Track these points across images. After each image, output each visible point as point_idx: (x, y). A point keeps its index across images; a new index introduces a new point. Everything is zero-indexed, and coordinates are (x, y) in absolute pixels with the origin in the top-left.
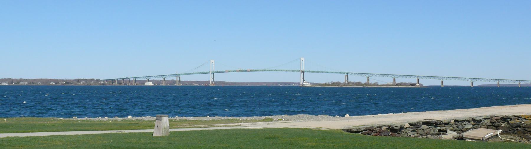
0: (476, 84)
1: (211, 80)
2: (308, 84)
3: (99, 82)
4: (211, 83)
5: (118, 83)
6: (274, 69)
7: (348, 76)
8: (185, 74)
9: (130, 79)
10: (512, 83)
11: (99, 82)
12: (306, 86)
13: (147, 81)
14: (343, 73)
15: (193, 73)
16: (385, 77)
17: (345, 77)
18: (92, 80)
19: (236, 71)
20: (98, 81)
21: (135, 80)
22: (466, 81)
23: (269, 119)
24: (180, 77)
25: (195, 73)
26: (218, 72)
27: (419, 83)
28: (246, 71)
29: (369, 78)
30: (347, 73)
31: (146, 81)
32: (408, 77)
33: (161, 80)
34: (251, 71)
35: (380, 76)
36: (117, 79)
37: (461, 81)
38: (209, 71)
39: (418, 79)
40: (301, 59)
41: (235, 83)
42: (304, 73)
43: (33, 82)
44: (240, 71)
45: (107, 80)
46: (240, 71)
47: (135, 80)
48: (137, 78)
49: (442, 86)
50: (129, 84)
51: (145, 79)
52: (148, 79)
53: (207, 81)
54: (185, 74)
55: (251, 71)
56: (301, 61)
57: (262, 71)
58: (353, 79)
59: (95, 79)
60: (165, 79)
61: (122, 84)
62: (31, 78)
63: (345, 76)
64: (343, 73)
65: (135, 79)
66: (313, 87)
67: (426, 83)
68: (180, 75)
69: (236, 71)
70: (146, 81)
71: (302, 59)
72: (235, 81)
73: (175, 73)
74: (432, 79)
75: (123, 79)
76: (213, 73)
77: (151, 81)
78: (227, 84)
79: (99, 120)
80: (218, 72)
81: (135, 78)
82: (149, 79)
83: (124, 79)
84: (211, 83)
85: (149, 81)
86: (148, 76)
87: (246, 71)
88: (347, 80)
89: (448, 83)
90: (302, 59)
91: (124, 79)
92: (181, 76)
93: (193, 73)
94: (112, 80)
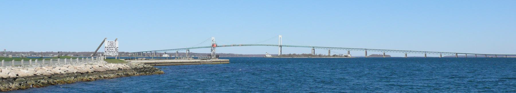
0: (443, 56)
2: (269, 55)
3: (128, 55)
5: (143, 55)
6: (198, 47)
7: (314, 49)
8: (193, 48)
9: (148, 52)
10: (451, 55)
11: (128, 55)
12: (268, 57)
13: (165, 54)
14: (311, 47)
15: (199, 48)
16: (342, 50)
17: (312, 50)
18: (123, 53)
19: (230, 46)
20: (127, 53)
21: (156, 53)
22: (401, 53)
24: (189, 50)
25: (263, 45)
26: (284, 46)
28: (238, 46)
29: (330, 51)
30: (313, 47)
31: (163, 54)
32: (392, 51)
34: (242, 45)
35: (369, 51)
36: (142, 52)
37: (398, 53)
38: (278, 45)
39: (366, 52)
40: (279, 36)
41: (242, 55)
42: (281, 47)
43: (77, 54)
44: (234, 46)
45: (134, 53)
46: (234, 46)
47: (156, 53)
48: (157, 51)
49: (366, 57)
52: (165, 51)
54: (193, 48)
55: (242, 45)
56: (279, 38)
57: (250, 45)
58: (318, 52)
59: (125, 52)
61: (146, 55)
62: (77, 51)
63: (312, 49)
64: (311, 47)
65: (155, 52)
66: (273, 57)
67: (355, 54)
68: (189, 49)
69: (230, 46)
70: (163, 54)
71: (280, 36)
72: (241, 54)
74: (359, 51)
76: (281, 46)
77: (167, 54)
78: (234, 56)
79: (93, 76)
80: (284, 46)
81: (156, 51)
82: (166, 52)
83: (143, 53)
85: (166, 53)
87: (238, 46)
88: (313, 52)
90: (280, 36)
93: (199, 48)
94: (139, 53)
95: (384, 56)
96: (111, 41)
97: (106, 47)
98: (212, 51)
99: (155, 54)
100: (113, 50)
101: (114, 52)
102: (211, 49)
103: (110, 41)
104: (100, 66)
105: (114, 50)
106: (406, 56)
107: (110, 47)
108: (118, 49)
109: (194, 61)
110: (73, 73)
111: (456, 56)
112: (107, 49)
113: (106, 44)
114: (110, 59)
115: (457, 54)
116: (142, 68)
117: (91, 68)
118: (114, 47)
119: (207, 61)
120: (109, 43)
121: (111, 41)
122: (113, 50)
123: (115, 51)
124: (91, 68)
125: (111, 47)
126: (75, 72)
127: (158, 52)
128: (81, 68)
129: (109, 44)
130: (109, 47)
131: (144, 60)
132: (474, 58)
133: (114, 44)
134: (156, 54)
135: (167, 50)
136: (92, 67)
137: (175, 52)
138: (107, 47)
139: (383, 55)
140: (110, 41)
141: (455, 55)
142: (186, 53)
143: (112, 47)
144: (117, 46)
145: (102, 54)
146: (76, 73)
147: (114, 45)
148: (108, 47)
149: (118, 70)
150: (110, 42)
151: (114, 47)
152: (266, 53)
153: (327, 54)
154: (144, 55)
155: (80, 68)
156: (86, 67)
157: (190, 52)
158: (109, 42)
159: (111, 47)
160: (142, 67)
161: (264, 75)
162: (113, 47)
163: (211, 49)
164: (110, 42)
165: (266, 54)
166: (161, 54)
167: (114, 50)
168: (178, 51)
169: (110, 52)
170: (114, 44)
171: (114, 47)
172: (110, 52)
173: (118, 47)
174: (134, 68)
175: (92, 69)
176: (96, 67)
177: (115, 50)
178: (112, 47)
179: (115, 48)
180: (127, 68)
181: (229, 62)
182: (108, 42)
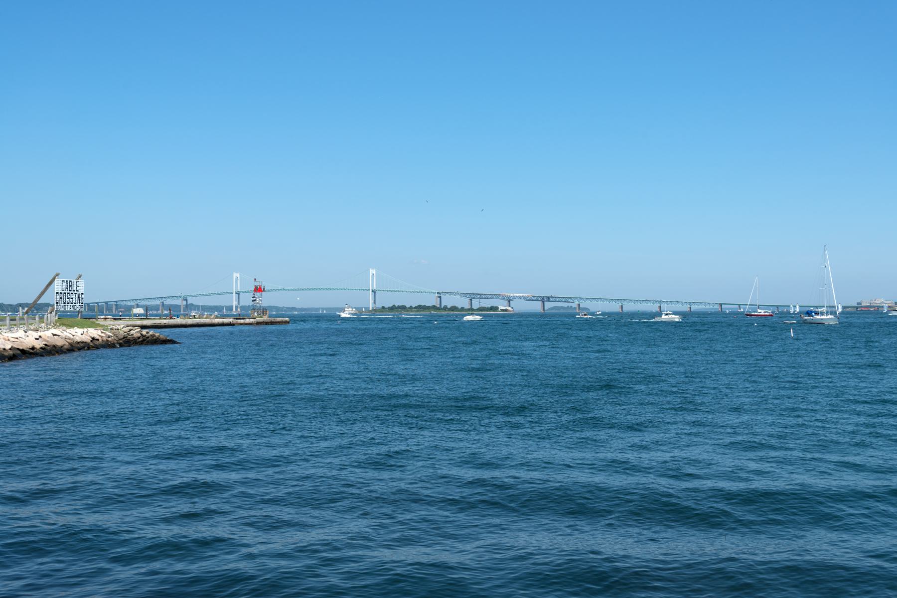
1: (235, 303)
4: (234, 309)
7: (440, 297)
13: (135, 307)
17: (436, 299)
23: (302, 311)
27: (511, 305)
31: (132, 307)
33: (157, 305)
40: (371, 271)
47: (116, 305)
50: (106, 312)
51: (133, 303)
53: (230, 306)
54: (192, 296)
60: (163, 303)
68: (187, 297)
71: (373, 271)
73: (179, 294)
75: (106, 303)
76: (238, 293)
80: (243, 292)
81: (116, 302)
83: (100, 304)
84: (234, 309)
85: (138, 306)
86: (162, 297)
89: (629, 307)
91: (90, 305)
92: (188, 298)
95: (577, 310)
96: (68, 280)
97: (57, 293)
98: (254, 301)
99: (114, 307)
100: (72, 298)
101: (75, 303)
102: (253, 297)
103: (65, 280)
104: (54, 335)
105: (74, 300)
106: (622, 310)
107: (67, 292)
108: (83, 296)
109: (220, 323)
110: (4, 349)
111: (720, 309)
112: (61, 298)
113: (58, 286)
114: (66, 319)
115: (721, 305)
116: (139, 338)
117: (38, 339)
118: (76, 294)
119: (246, 322)
120: (64, 284)
121: (68, 280)
122: (72, 298)
123: (76, 302)
124: (38, 339)
125: (68, 293)
126: (8, 347)
127: (122, 303)
128: (17, 338)
129: (64, 287)
130: (65, 293)
131: (111, 321)
132: (705, 314)
133: (75, 285)
134: (116, 309)
135: (140, 299)
136: (40, 337)
137: (158, 302)
138: (61, 293)
139: (575, 308)
140: (65, 280)
141: (717, 307)
142: (180, 305)
143: (70, 292)
144: (81, 290)
145: (838, 321)
146: (10, 349)
147: (75, 289)
148: (63, 292)
149: (91, 341)
150: (67, 282)
151: (74, 292)
152: (347, 306)
153: (619, 310)
154: (109, 309)
155: (16, 340)
156: (28, 336)
157: (188, 303)
158: (63, 281)
159: (69, 292)
160: (139, 335)
161: (866, 369)
162: (72, 292)
163: (253, 297)
164: (67, 282)
165: (347, 308)
166: (129, 309)
167: (74, 298)
168: (164, 302)
169: (66, 304)
170: (75, 285)
171: (74, 292)
172: (66, 304)
173: (82, 294)
174: (122, 337)
175: (40, 339)
176: (48, 337)
177: (77, 298)
178: (70, 292)
179: (77, 295)
180: (109, 337)
181: (99, 317)
182: (63, 281)
